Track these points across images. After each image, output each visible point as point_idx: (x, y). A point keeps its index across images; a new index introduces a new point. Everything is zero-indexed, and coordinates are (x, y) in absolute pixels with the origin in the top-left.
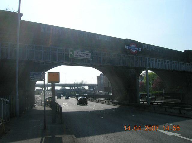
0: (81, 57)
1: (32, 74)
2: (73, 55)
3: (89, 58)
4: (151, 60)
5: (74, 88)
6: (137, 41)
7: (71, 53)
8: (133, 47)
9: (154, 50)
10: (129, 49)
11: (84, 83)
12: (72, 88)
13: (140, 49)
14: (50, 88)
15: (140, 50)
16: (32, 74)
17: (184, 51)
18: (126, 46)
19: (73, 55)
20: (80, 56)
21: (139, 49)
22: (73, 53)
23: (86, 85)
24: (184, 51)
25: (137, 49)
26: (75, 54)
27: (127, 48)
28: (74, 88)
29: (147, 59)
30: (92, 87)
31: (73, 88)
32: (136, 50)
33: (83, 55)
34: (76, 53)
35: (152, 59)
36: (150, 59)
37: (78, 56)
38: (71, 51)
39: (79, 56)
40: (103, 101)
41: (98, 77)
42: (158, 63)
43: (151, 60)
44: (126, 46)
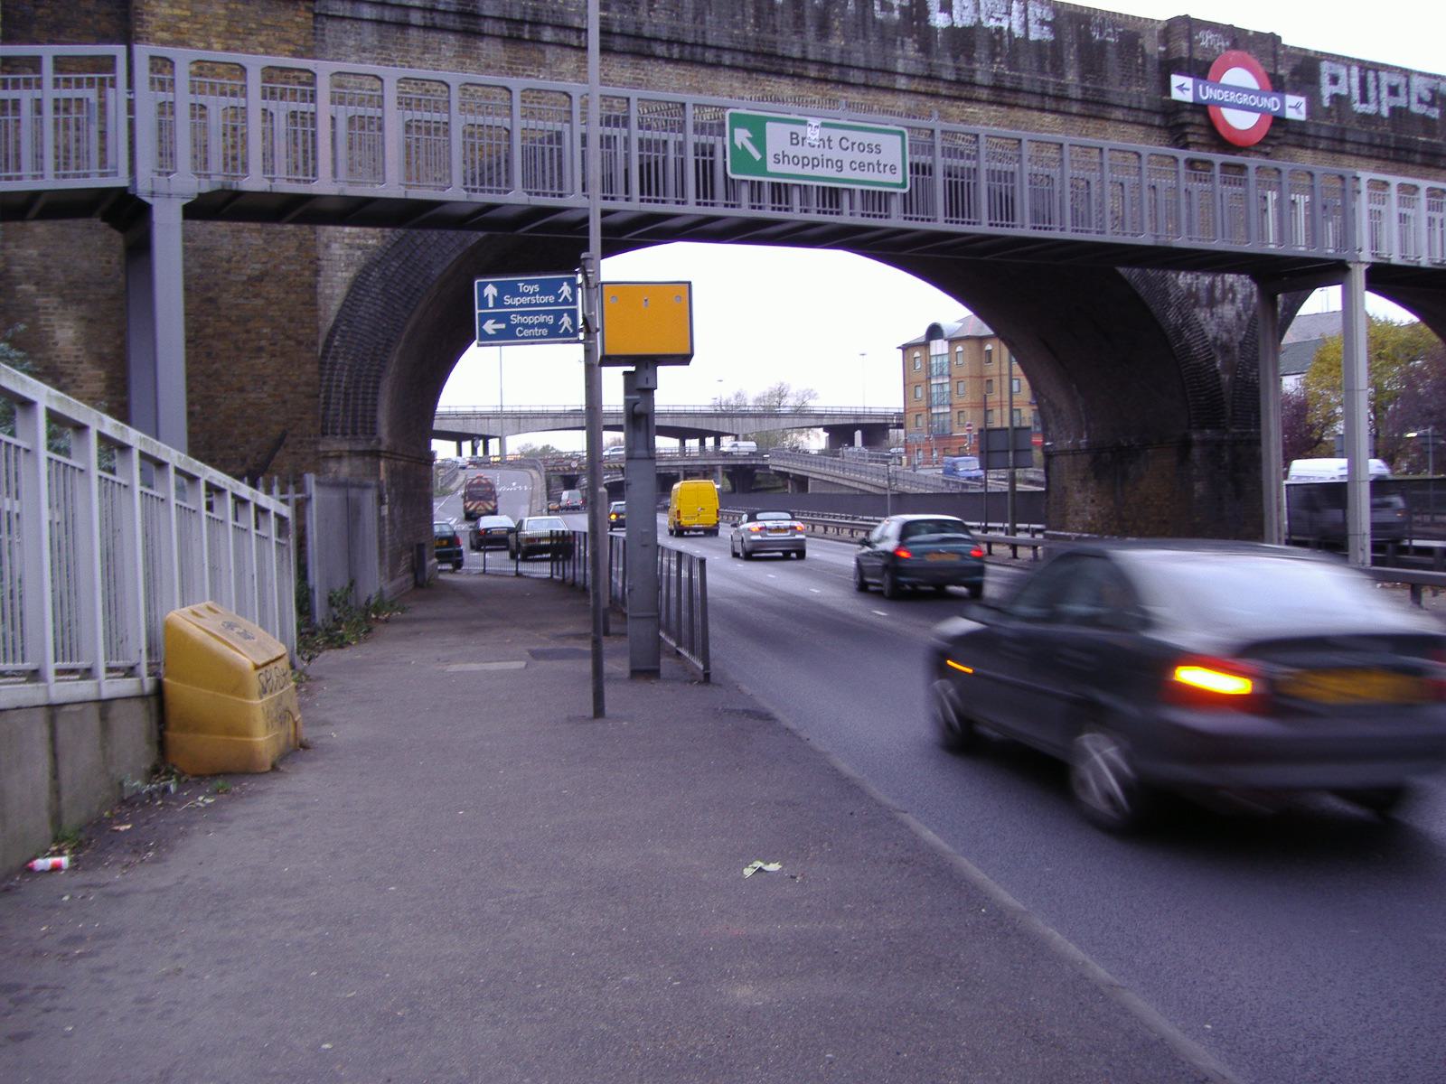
0: (819, 172)
1: (491, 291)
2: (758, 157)
3: (887, 177)
6: (1274, 39)
7: (742, 136)
8: (1237, 89)
9: (1416, 108)
10: (1200, 108)
12: (693, 444)
13: (1295, 107)
16: (491, 291)
18: (1176, 80)
19: (758, 157)
21: (1291, 100)
22: (759, 141)
23: (804, 417)
25: (1271, 103)
27: (1187, 97)
28: (710, 442)
29: (1363, 185)
30: (858, 435)
31: (702, 443)
32: (1263, 111)
33: (835, 154)
34: (777, 136)
35: (1402, 187)
36: (1386, 184)
37: (795, 160)
38: (738, 121)
39: (804, 162)
40: (1014, 547)
41: (906, 348)
42: (1431, 221)
44: (1176, 80)
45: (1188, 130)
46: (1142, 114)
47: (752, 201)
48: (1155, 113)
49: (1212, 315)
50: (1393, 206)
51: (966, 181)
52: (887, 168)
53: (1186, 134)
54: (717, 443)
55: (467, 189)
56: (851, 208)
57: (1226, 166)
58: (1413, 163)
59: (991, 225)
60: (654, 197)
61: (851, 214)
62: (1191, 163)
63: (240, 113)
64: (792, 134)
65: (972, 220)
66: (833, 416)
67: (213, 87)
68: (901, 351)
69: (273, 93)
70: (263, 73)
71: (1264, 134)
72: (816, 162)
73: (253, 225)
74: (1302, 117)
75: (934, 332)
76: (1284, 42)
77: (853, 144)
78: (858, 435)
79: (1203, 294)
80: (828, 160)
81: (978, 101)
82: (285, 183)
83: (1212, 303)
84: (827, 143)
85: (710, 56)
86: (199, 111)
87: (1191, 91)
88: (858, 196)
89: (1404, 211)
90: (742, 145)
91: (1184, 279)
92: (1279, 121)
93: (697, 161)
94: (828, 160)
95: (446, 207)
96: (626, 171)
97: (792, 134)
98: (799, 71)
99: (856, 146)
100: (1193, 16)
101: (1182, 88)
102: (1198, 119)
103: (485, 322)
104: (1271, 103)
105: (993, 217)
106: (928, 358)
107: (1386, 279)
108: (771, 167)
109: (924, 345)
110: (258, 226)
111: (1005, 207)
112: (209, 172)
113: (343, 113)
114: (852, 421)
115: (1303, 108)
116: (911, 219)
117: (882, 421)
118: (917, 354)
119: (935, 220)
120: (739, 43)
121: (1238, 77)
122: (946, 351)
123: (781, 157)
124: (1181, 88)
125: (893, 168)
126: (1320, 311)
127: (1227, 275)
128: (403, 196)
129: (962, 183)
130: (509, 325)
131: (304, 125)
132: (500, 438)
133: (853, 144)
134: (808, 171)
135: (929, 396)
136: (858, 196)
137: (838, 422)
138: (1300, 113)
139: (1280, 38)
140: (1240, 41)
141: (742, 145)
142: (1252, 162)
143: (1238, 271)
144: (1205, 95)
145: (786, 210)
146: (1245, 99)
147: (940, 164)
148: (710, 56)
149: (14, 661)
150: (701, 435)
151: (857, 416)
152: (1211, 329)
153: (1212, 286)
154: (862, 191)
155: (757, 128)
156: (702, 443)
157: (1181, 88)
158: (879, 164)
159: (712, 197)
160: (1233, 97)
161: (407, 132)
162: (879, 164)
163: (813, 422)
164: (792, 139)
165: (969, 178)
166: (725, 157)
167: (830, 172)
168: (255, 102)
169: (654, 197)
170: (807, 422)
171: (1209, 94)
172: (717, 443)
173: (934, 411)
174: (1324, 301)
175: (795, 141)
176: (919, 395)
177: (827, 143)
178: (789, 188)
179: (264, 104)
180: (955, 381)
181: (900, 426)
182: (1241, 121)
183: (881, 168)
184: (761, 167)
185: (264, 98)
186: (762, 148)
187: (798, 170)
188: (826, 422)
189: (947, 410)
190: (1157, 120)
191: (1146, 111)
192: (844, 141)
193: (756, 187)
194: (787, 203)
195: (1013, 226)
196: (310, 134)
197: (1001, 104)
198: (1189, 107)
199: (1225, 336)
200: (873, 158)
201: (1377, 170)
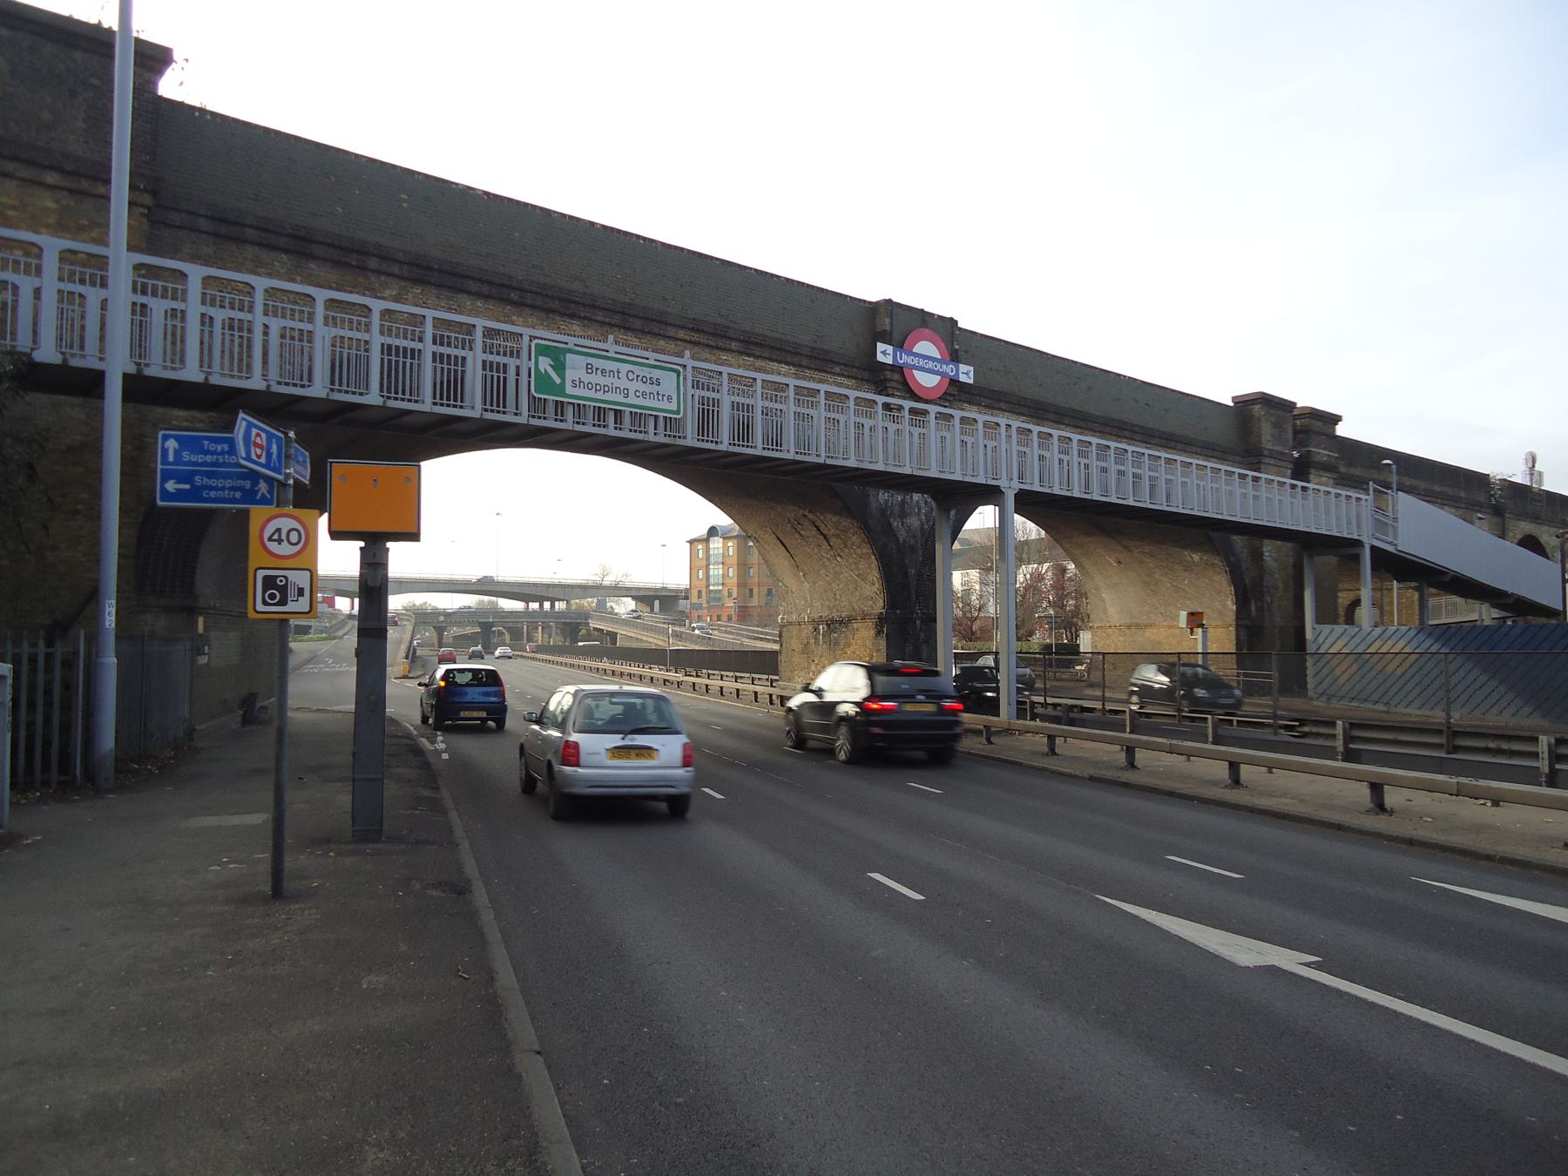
2: (558, 381)
4: (1075, 444)
5: (547, 605)
6: (953, 322)
10: (898, 369)
11: (608, 581)
12: (534, 606)
13: (966, 374)
14: (226, 456)
15: (963, 378)
17: (1234, 398)
18: (880, 347)
19: (558, 381)
20: (606, 389)
21: (963, 368)
23: (619, 591)
24: (1234, 398)
26: (570, 375)
27: (889, 360)
28: (547, 605)
30: (657, 603)
31: (541, 606)
34: (575, 367)
39: (597, 387)
41: (691, 542)
43: (1075, 444)
44: (880, 347)
45: (888, 385)
46: (855, 370)
47: (435, 398)
48: (865, 370)
49: (902, 524)
50: (1054, 454)
51: (711, 408)
52: (665, 398)
53: (887, 387)
54: (553, 606)
55: (383, 396)
56: (655, 429)
57: (913, 411)
58: (1047, 420)
59: (764, 449)
60: (706, 438)
61: (655, 434)
62: (887, 407)
63: (178, 315)
64: (587, 364)
65: (750, 444)
66: (639, 589)
67: (351, 322)
68: (688, 544)
69: (390, 330)
70: (325, 304)
71: (942, 392)
72: (606, 389)
73: (74, 400)
74: (971, 381)
75: (713, 531)
76: (959, 325)
77: (638, 376)
78: (657, 603)
79: (897, 508)
80: (616, 388)
81: (731, 351)
82: (218, 376)
83: (903, 515)
84: (616, 374)
85: (514, 296)
86: (207, 320)
87: (960, 372)
88: (661, 422)
89: (1184, 480)
90: (545, 370)
91: (883, 496)
92: (954, 382)
93: (382, 359)
94: (616, 388)
95: (405, 419)
96: (35, 324)
97: (587, 364)
98: (589, 315)
99: (639, 378)
100: (926, 310)
101: (885, 353)
102: (896, 377)
103: (166, 482)
104: (949, 369)
105: (732, 439)
106: (708, 549)
107: (1030, 504)
108: (569, 390)
109: (706, 540)
110: (80, 400)
111: (743, 431)
112: (85, 353)
113: (276, 325)
114: (652, 593)
115: (971, 374)
116: (703, 440)
117: (674, 594)
118: (700, 547)
119: (685, 437)
120: (540, 288)
121: (926, 347)
122: (721, 545)
123: (578, 383)
124: (884, 353)
125: (669, 398)
126: (978, 527)
127: (914, 494)
128: (856, 466)
129: (708, 410)
130: (193, 486)
131: (442, 363)
132: (567, 602)
133: (638, 376)
134: (600, 395)
135: (708, 577)
136: (661, 422)
137: (642, 593)
138: (969, 378)
139: (956, 322)
140: (922, 321)
141: (545, 370)
142: (933, 409)
143: (1239, 534)
144: (901, 359)
145: (561, 421)
146: (930, 365)
147: (76, 307)
148: (514, 296)
149: (1333, 736)
150: (541, 600)
151: (656, 590)
152: (902, 535)
153: (903, 501)
154: (631, 412)
155: (558, 357)
156: (541, 606)
157: (884, 353)
158: (658, 394)
159: (504, 407)
160: (930, 365)
161: (133, 314)
162: (658, 394)
163: (625, 593)
164: (587, 368)
165: (714, 406)
166: (530, 377)
167: (620, 398)
168: (194, 308)
169: (706, 438)
170: (620, 593)
171: (904, 359)
172: (553, 606)
173: (711, 588)
174: (983, 518)
175: (590, 371)
176: (701, 576)
177: (616, 374)
178: (565, 405)
179: (203, 309)
180: (726, 567)
181: (686, 598)
182: (927, 380)
183: (660, 397)
184: (560, 390)
185: (203, 303)
186: (563, 378)
187: (591, 394)
188: (633, 593)
189: (720, 588)
190: (866, 375)
191: (858, 368)
192: (630, 373)
193: (560, 406)
194: (562, 416)
195: (781, 451)
196: (245, 338)
197: (749, 355)
198: (889, 367)
199: (912, 541)
200: (655, 388)
201: (1081, 434)
